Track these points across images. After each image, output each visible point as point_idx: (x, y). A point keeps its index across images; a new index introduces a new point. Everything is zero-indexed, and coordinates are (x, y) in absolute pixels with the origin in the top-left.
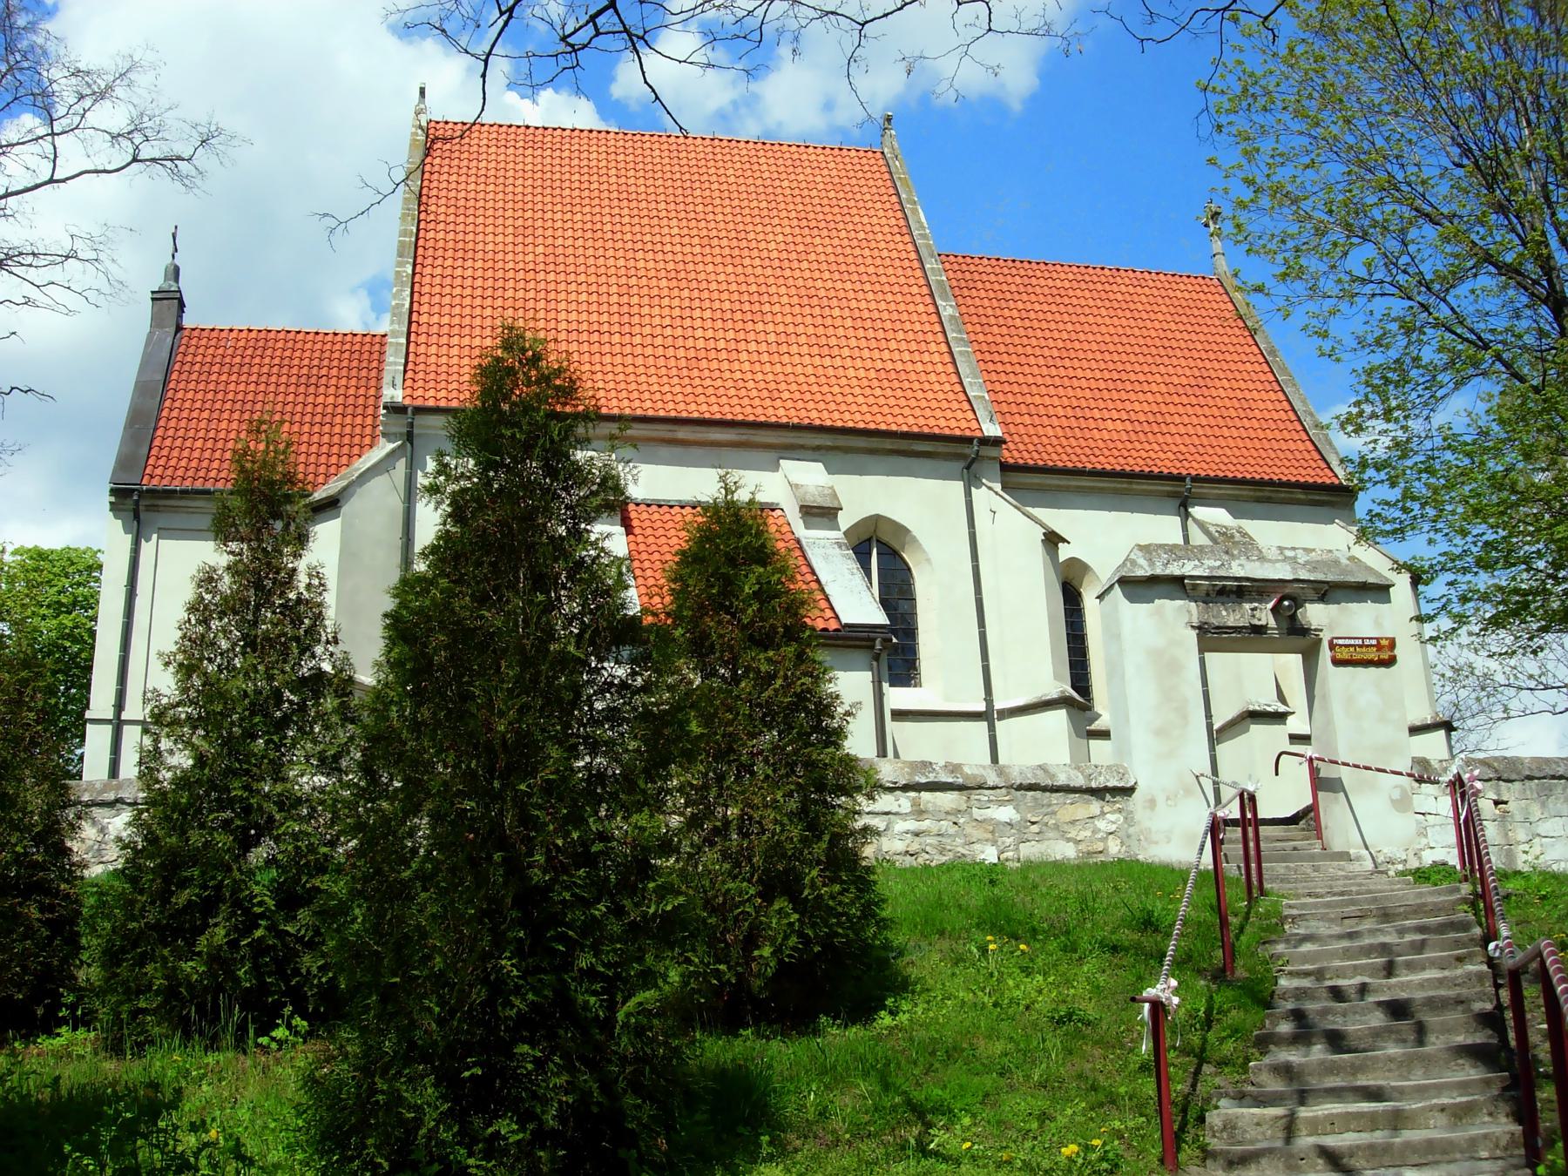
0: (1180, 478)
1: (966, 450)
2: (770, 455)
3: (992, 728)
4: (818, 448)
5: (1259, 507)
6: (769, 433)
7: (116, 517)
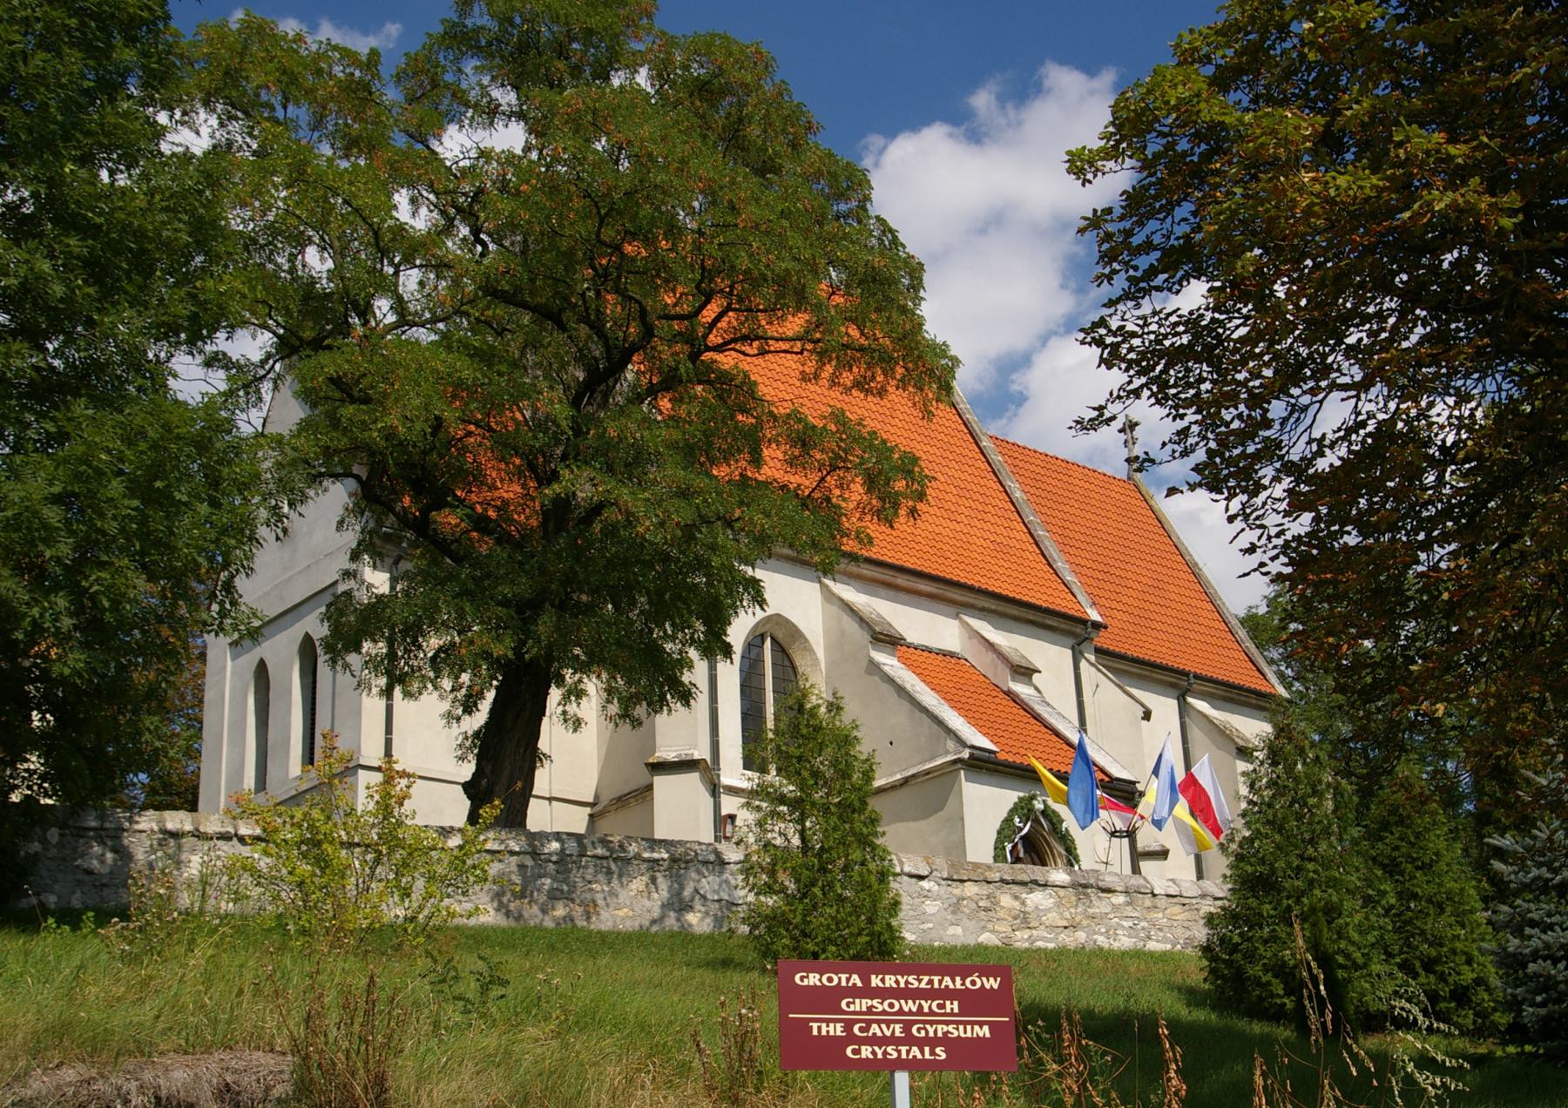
0: (1185, 674)
1: (1079, 630)
3: (388, 753)
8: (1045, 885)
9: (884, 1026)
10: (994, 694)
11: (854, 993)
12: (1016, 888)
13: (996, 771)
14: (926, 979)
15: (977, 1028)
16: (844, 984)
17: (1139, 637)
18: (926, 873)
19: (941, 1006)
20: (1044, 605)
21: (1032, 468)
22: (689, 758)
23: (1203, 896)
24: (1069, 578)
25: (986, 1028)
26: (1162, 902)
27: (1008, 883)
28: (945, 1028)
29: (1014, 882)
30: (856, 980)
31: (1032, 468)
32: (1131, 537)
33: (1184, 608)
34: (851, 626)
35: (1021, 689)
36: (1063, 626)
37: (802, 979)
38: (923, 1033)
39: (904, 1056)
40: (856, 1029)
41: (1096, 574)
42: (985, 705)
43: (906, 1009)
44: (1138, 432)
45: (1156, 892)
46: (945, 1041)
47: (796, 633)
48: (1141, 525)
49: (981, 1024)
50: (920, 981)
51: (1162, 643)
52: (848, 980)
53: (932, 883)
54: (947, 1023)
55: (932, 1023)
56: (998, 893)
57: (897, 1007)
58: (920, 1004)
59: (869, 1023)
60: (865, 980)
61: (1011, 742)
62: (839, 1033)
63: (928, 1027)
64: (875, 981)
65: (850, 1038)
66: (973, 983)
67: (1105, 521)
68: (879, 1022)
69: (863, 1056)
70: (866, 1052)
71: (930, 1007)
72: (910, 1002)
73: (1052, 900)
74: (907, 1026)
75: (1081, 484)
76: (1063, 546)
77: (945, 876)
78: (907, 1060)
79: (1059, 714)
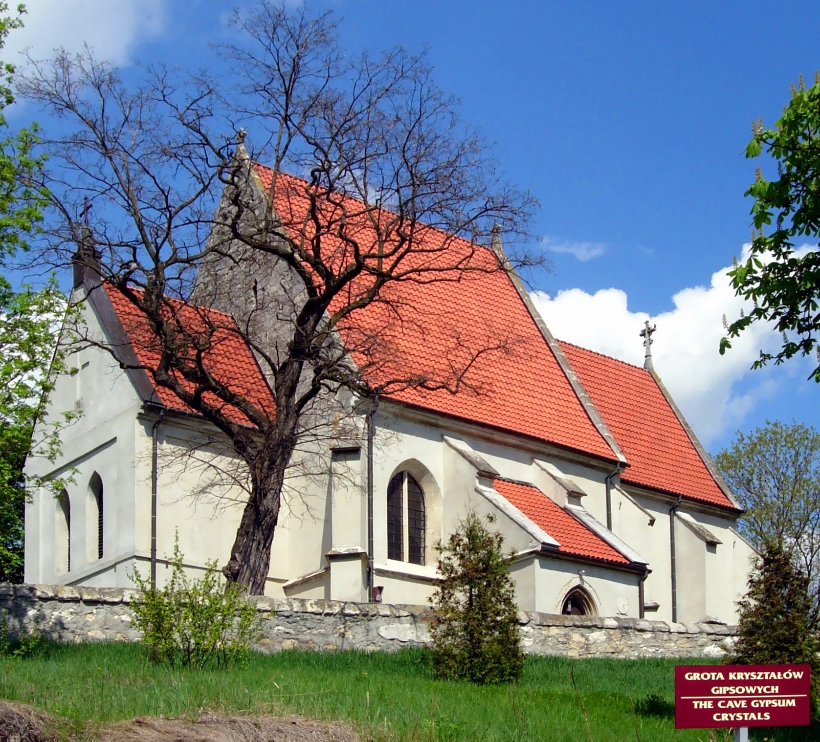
0: (676, 495)
1: (611, 467)
2: (528, 455)
3: (154, 550)
4: (549, 455)
5: (421, 427)
6: (535, 443)
7: (141, 424)
8: (602, 628)
9: (735, 702)
10: (555, 509)
11: (719, 683)
12: (583, 630)
13: (557, 558)
14: (761, 674)
15: (788, 701)
16: (713, 678)
17: (647, 472)
18: (524, 621)
19: (768, 690)
20: (590, 452)
21: (582, 360)
22: (355, 551)
23: (701, 632)
24: (606, 434)
25: (793, 701)
26: (674, 637)
27: (578, 627)
28: (770, 702)
29: (582, 627)
30: (721, 676)
31: (582, 360)
32: (645, 406)
33: (677, 453)
34: (464, 465)
35: (573, 508)
36: (601, 465)
37: (689, 676)
38: (757, 705)
39: (746, 718)
40: (719, 705)
41: (621, 431)
42: (550, 516)
43: (749, 692)
44: (654, 336)
45: (671, 631)
46: (770, 709)
47: (424, 471)
48: (651, 399)
49: (791, 699)
50: (757, 675)
51: (662, 476)
52: (716, 676)
53: (529, 628)
54: (771, 699)
55: (762, 699)
56: (571, 633)
57: (743, 691)
58: (757, 689)
59: (727, 700)
60: (726, 676)
61: (567, 540)
62: (709, 707)
63: (760, 701)
64: (732, 676)
65: (716, 710)
66: (788, 675)
67: (628, 396)
68: (732, 700)
69: (723, 719)
70: (725, 717)
71: (762, 691)
72: (751, 688)
73: (605, 637)
74: (749, 701)
75: (614, 371)
76: (603, 411)
77: (538, 623)
78: (748, 721)
79: (598, 522)
